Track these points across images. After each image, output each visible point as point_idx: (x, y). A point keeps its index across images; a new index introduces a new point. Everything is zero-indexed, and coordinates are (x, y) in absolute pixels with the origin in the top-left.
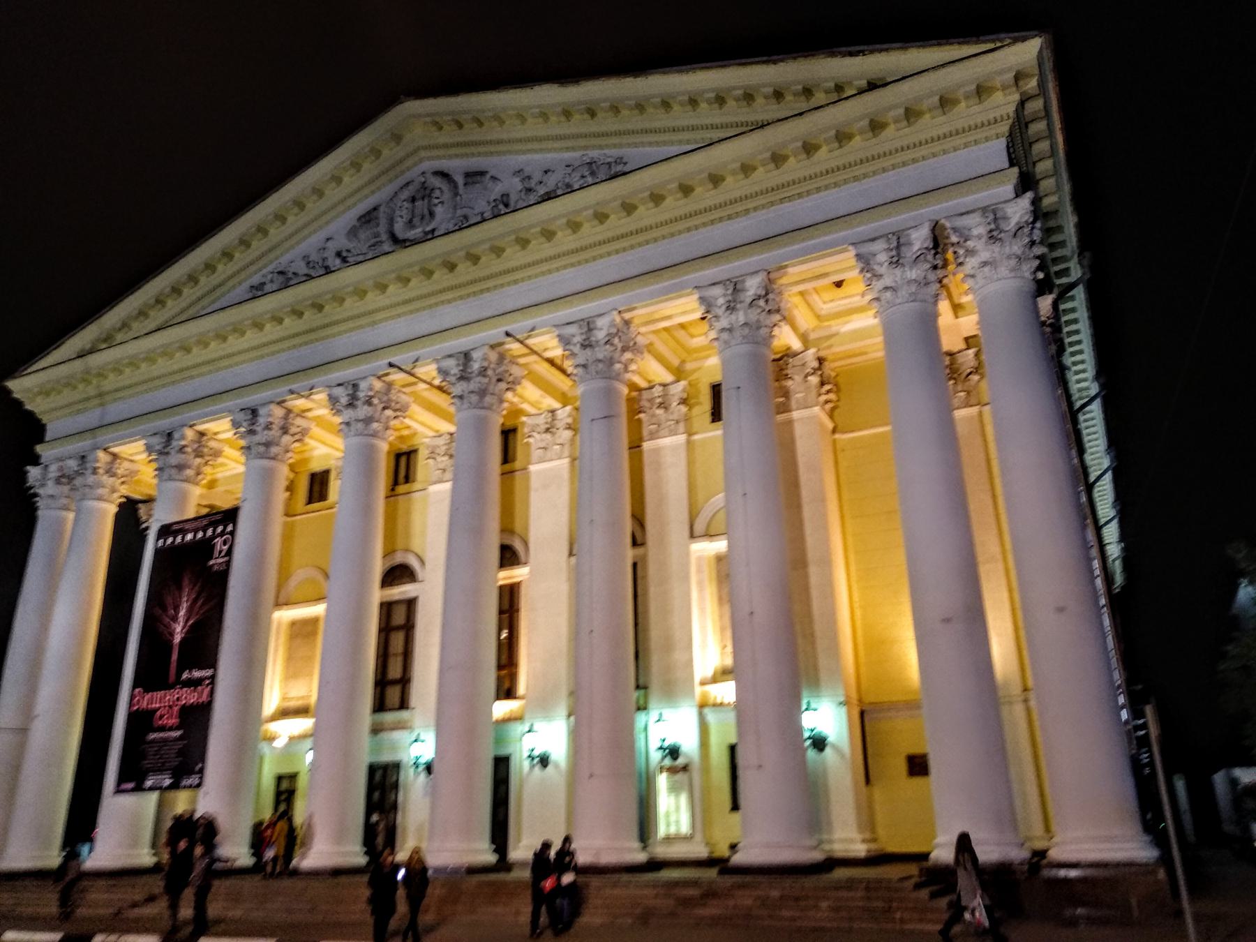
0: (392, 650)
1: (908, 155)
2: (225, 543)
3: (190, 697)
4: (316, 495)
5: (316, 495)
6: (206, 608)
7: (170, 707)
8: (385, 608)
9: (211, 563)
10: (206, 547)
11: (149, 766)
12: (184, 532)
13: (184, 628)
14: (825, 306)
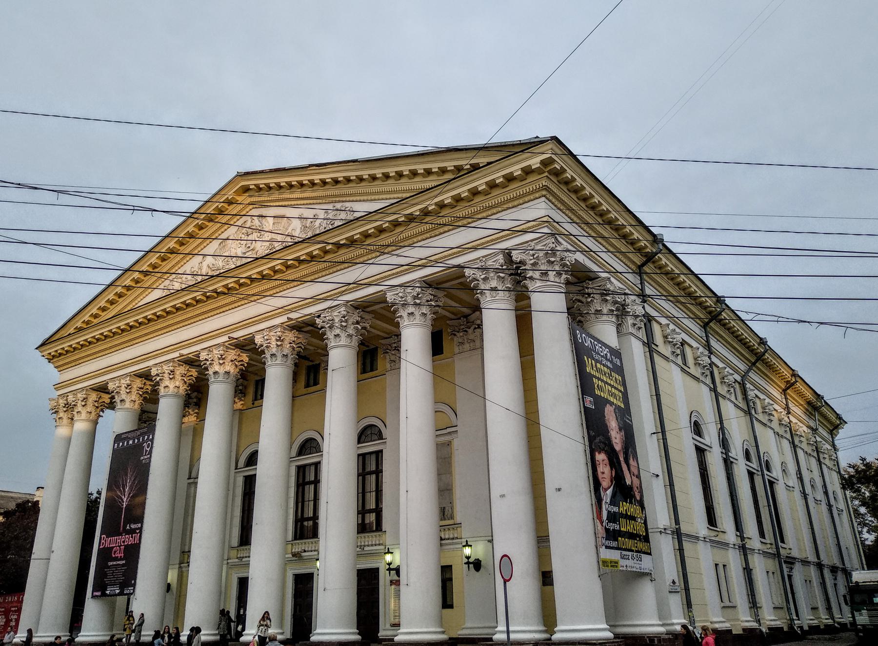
0: (368, 489)
3: (129, 540)
4: (312, 382)
5: (312, 382)
7: (119, 546)
8: (361, 458)
9: (142, 458)
12: (128, 439)
13: (127, 499)
14: (544, 182)
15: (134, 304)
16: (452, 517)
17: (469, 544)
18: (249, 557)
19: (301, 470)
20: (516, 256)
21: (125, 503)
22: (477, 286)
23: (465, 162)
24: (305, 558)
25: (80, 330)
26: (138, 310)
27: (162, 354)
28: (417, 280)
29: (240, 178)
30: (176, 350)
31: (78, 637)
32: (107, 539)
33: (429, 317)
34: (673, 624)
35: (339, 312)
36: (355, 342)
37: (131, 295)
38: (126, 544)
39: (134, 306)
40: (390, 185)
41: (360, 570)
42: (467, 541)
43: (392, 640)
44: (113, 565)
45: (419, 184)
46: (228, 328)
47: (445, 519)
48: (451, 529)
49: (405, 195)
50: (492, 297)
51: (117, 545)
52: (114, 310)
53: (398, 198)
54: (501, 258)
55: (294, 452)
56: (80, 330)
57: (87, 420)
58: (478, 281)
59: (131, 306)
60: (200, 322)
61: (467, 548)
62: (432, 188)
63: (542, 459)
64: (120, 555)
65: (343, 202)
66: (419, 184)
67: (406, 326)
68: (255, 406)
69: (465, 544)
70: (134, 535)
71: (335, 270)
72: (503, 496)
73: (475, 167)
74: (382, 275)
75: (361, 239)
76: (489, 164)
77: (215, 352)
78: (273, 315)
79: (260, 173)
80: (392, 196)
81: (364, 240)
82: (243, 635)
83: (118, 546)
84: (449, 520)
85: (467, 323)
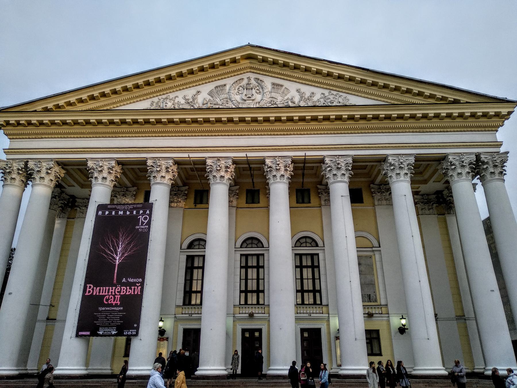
1: (449, 319)
2: (145, 219)
6: (135, 249)
10: (135, 220)
11: (98, 324)
15: (115, 106)
16: (376, 301)
17: (404, 317)
18: (201, 314)
19: (190, 259)
20: (31, 164)
21: (117, 261)
22: (92, 173)
23: (451, 97)
24: (256, 318)
25: (47, 110)
27: (224, 151)
29: (250, 48)
30: (46, 153)
31: (197, 370)
32: (95, 288)
33: (54, 182)
34: (27, 370)
36: (52, 185)
37: (114, 98)
38: (122, 293)
39: (114, 108)
40: (385, 93)
42: (402, 316)
44: (105, 310)
47: (371, 302)
48: (247, 308)
51: (110, 294)
52: (92, 105)
53: (387, 102)
54: (474, 158)
55: (238, 244)
56: (47, 110)
57: (49, 187)
58: (34, 171)
60: (168, 138)
61: (403, 320)
62: (417, 104)
63: (86, 277)
64: (115, 302)
65: (338, 91)
67: (213, 184)
68: (196, 207)
69: (401, 317)
70: (133, 288)
72: (493, 291)
73: (456, 102)
74: (376, 145)
75: (119, 123)
76: (467, 102)
77: (44, 164)
79: (273, 50)
82: (197, 370)
83: (112, 295)
85: (178, 190)
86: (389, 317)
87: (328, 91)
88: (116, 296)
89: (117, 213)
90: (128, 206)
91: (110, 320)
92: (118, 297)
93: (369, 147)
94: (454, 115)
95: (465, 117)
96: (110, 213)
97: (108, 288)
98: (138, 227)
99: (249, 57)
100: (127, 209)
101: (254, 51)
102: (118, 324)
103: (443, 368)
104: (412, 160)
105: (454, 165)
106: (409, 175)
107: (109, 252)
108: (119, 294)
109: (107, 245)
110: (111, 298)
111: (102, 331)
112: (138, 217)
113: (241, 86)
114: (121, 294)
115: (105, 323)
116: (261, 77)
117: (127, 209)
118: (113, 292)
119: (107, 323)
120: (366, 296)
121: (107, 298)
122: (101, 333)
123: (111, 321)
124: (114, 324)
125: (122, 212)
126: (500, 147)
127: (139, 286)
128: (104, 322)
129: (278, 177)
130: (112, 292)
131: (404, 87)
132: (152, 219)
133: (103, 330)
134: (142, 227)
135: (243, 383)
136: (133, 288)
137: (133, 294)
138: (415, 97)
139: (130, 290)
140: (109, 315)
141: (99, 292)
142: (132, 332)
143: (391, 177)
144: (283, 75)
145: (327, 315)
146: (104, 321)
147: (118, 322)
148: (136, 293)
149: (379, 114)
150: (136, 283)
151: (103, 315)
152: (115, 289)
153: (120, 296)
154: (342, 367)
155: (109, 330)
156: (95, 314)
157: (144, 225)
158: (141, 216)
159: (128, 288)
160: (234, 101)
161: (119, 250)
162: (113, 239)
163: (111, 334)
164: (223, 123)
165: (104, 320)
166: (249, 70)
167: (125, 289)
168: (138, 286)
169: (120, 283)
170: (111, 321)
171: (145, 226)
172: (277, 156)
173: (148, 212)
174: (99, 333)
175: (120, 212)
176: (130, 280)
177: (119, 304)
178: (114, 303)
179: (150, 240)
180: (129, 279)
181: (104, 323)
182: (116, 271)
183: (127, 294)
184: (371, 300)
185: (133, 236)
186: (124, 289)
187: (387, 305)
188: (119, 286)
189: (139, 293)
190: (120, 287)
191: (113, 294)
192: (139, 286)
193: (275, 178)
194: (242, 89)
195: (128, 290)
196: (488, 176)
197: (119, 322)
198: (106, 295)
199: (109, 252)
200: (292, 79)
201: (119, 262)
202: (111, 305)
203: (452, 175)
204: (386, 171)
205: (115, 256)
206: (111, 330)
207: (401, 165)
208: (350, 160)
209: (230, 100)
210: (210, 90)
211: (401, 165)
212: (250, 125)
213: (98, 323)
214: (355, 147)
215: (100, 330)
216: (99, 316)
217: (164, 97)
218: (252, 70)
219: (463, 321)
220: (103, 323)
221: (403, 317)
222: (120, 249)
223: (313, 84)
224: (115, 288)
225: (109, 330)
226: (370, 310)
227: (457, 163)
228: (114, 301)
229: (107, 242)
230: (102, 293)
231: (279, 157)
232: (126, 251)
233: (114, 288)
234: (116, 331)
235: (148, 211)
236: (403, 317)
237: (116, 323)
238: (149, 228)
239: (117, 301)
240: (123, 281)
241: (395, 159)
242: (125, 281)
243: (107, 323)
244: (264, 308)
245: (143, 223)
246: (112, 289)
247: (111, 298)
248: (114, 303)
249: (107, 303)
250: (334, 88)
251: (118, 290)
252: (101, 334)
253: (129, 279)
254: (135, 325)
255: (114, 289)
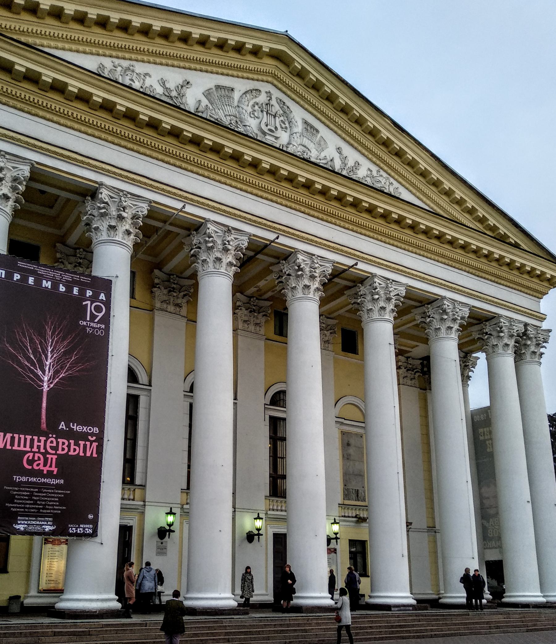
15: (45, 42)
17: (173, 511)
26: (105, 82)
27: (133, 182)
28: (32, 162)
30: (365, 261)
31: (504, 597)
35: (14, 168)
38: (60, 452)
41: (277, 534)
42: (335, 519)
43: (53, 607)
44: (27, 482)
45: (455, 212)
46: (350, 250)
47: (359, 500)
49: (442, 213)
50: (215, 268)
51: (35, 449)
59: (38, 41)
61: (258, 520)
65: (389, 175)
66: (455, 212)
71: (454, 265)
73: (516, 246)
78: (293, 234)
80: (428, 202)
81: (97, 109)
83: (39, 452)
84: (362, 501)
86: (145, 507)
87: (377, 168)
88: (48, 456)
89: (38, 282)
90: (61, 274)
91: (38, 502)
92: (52, 458)
93: (424, 278)
94: (263, 165)
95: (224, 155)
96: (24, 279)
97: (31, 437)
98: (85, 323)
99: (276, 56)
100: (60, 281)
101: (290, 49)
102: (56, 512)
103: (540, 594)
104: (144, 209)
105: (301, 270)
106: (132, 237)
107: (26, 363)
108: (54, 452)
109: (21, 348)
110: (39, 459)
111: (24, 524)
112: (84, 303)
113: (257, 104)
114: (58, 452)
115: (29, 508)
116: (289, 103)
117: (60, 281)
118: (42, 447)
119: (33, 508)
120: (354, 491)
121: (31, 458)
122: (21, 527)
123: (40, 505)
124: (49, 511)
125: (49, 283)
126: (542, 321)
127: (94, 441)
128: (28, 506)
129: (224, 264)
130: (39, 447)
131: (469, 203)
132: (112, 314)
133: (26, 523)
134: (92, 324)
135: (309, 619)
136: (82, 443)
137: (83, 455)
138: (474, 222)
139: (77, 448)
140: (36, 492)
141: (12, 444)
142: (84, 529)
143: (97, 229)
144: (316, 108)
145: (142, 503)
146: (27, 504)
147: (55, 507)
148: (88, 454)
149: (281, 167)
150: (88, 434)
151: (24, 491)
152: (46, 442)
153: (56, 457)
154: (64, 596)
155: (38, 523)
156: (7, 488)
157: (96, 321)
158: (89, 303)
159: (72, 442)
160: (248, 128)
161: (48, 363)
162: (34, 337)
163: (42, 531)
164: (294, 185)
165: (27, 502)
166: (270, 79)
167: (67, 443)
168: (91, 442)
169: (53, 428)
170: (40, 505)
171: (99, 325)
172: (457, 301)
173: (102, 297)
174: (17, 527)
175: (44, 282)
176: (75, 427)
177: (55, 473)
178: (45, 470)
179: (110, 354)
180: (73, 426)
181: (27, 508)
182: (44, 405)
183: (70, 453)
184: (359, 498)
185: (74, 338)
186: (63, 443)
187: (144, 486)
188: (52, 437)
189: (95, 455)
190: (56, 439)
191: (42, 450)
192: (94, 441)
193: (306, 290)
194: (258, 108)
195: (73, 447)
196: (528, 357)
197: (58, 509)
198: (28, 452)
199: (26, 363)
200: (332, 126)
201: (48, 387)
202: (39, 473)
203: (98, 227)
204: (432, 319)
205: (40, 373)
206: (43, 523)
207: (121, 213)
208: (26, 171)
209: (241, 122)
210: (207, 89)
211: (121, 213)
212: (19, 84)
213: (14, 507)
214: (409, 273)
215: (19, 522)
216: (15, 493)
217: (125, 63)
218: (276, 82)
219: (434, 533)
220: (24, 508)
221: (335, 521)
222: (49, 361)
223: (360, 148)
224: (45, 438)
225: (38, 523)
226: (357, 511)
227: (382, 292)
228: (45, 465)
229: (22, 342)
230: (19, 446)
231: (318, 256)
232: (62, 368)
233: (43, 439)
234: (53, 525)
235: (102, 295)
236: (335, 521)
237: (51, 509)
238: (107, 329)
239: (51, 466)
240: (61, 427)
241: (381, 284)
242: (64, 427)
243: (33, 508)
244: (134, 490)
245: (93, 317)
246: (39, 441)
247: (39, 459)
248: (45, 470)
249: (30, 467)
250: (386, 168)
251: (52, 445)
252: (22, 529)
253: (73, 426)
254: (90, 517)
255: (43, 442)
